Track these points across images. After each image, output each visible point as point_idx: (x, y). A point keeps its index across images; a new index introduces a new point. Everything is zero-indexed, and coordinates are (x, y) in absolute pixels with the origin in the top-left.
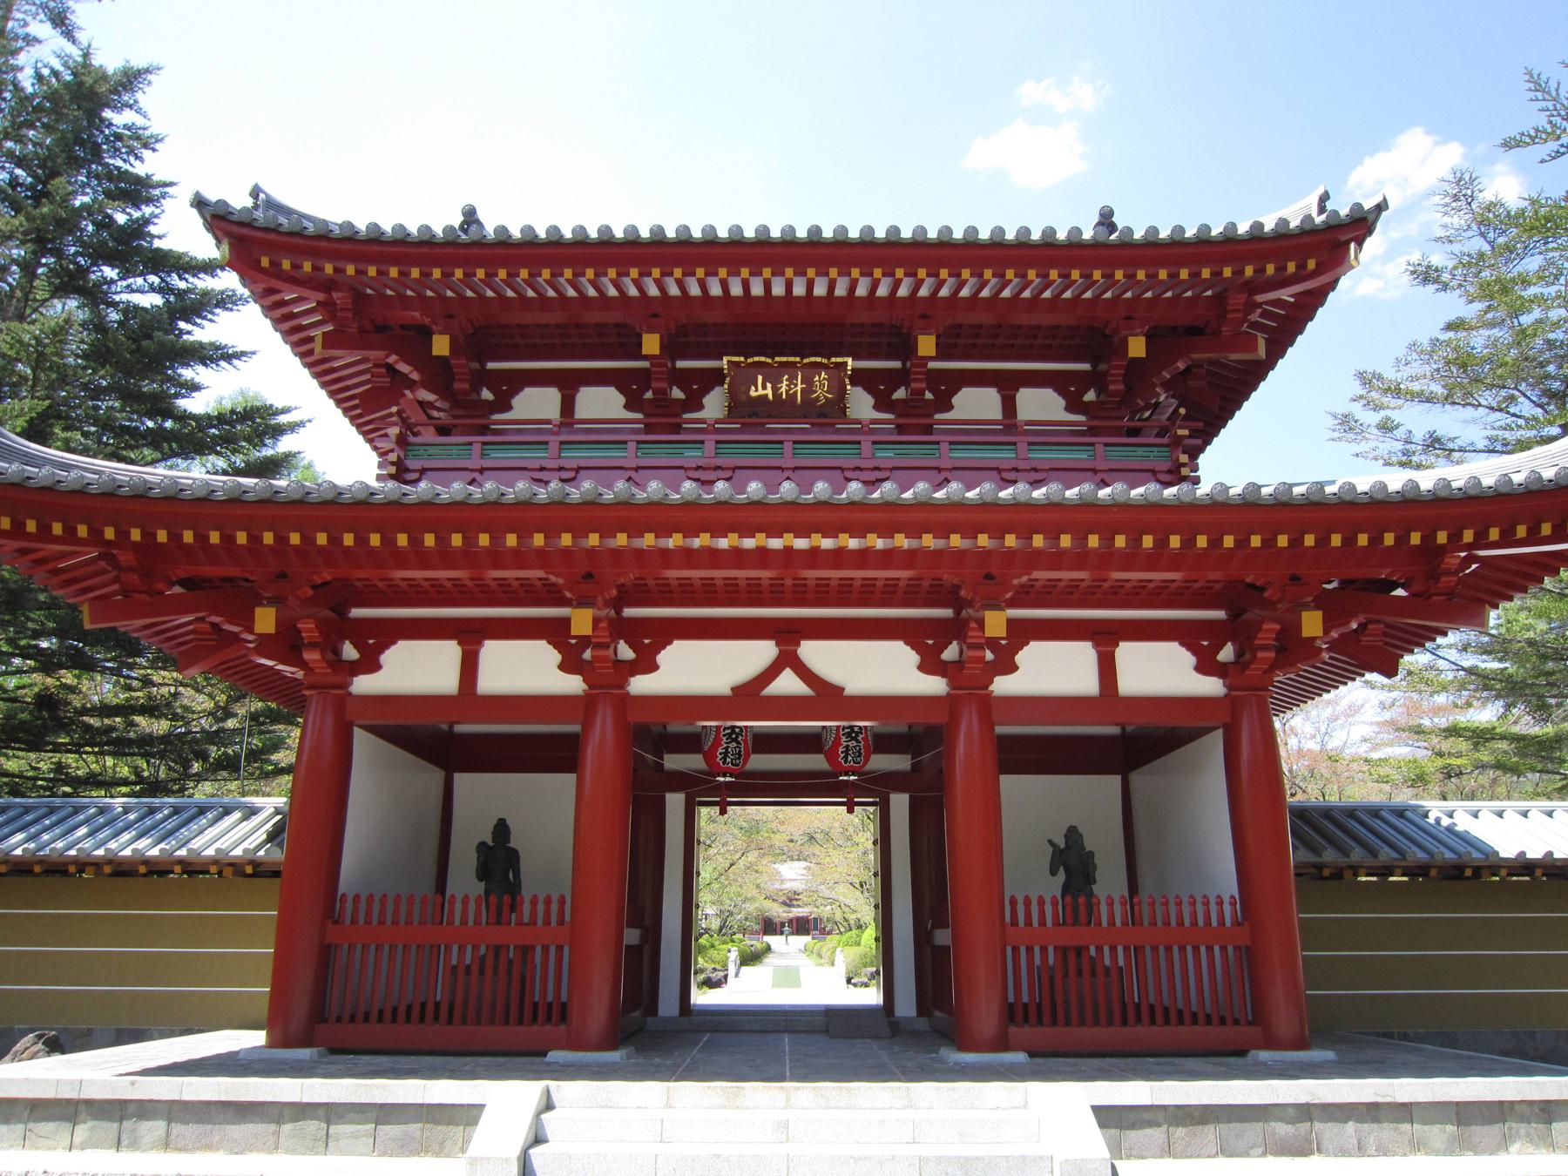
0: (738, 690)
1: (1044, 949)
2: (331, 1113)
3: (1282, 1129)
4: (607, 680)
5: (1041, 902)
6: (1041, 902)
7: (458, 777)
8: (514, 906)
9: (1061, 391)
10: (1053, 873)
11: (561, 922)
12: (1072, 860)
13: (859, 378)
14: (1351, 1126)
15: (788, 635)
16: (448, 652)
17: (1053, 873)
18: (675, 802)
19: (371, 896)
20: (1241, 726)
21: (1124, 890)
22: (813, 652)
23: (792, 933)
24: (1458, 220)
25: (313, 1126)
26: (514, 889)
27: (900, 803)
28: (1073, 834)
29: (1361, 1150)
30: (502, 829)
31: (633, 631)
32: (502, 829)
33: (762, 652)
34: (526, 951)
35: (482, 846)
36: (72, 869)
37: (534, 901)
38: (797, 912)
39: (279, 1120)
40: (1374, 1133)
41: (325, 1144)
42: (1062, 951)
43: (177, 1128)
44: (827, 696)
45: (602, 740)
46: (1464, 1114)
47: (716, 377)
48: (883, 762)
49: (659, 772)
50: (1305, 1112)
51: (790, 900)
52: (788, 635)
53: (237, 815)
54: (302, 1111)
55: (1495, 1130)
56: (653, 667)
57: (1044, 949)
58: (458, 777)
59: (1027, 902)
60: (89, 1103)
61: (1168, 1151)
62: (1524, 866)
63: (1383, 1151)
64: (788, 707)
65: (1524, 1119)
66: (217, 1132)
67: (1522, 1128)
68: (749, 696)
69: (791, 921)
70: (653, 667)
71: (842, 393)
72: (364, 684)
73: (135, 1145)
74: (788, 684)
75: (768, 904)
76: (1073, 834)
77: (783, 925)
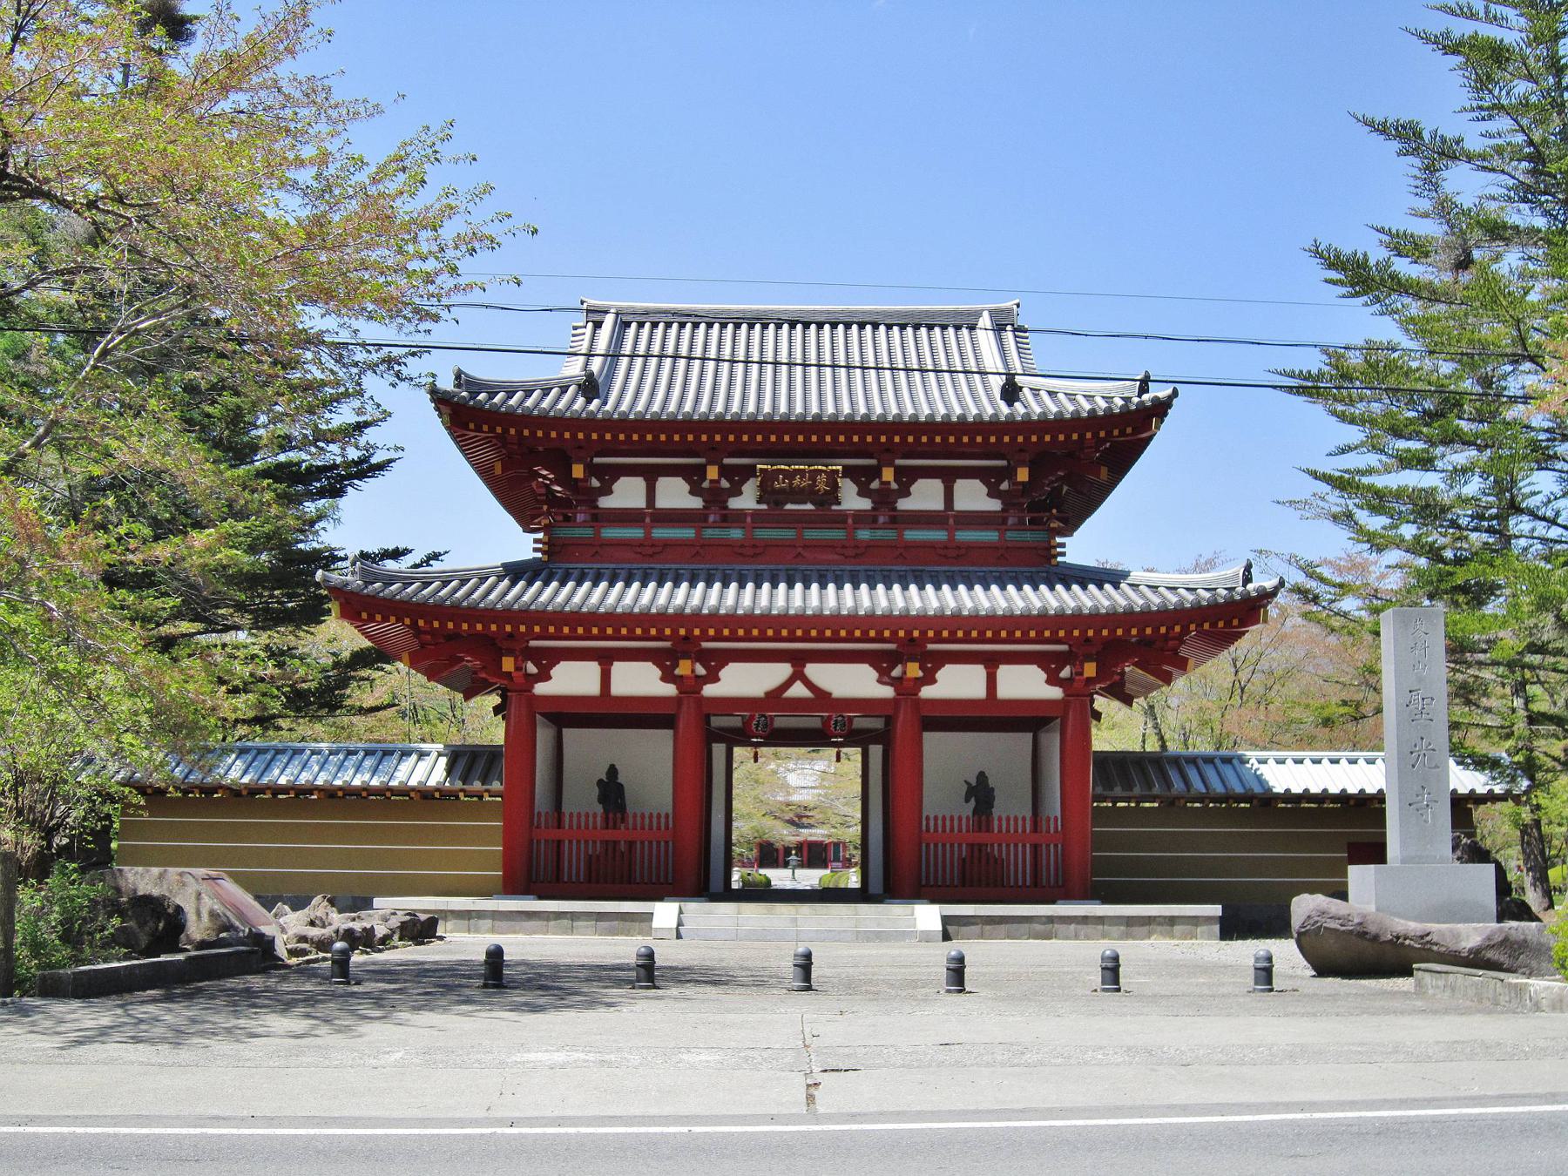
0: (768, 694)
1: (960, 846)
2: (574, 916)
3: (1038, 927)
4: (690, 687)
5: (960, 819)
6: (960, 819)
7: (565, 731)
8: (623, 820)
9: (985, 482)
10: (967, 801)
11: (667, 827)
12: (981, 793)
13: (849, 472)
14: (1073, 926)
15: (798, 660)
16: (592, 669)
17: (967, 801)
18: (719, 750)
19: (579, 815)
20: (1073, 715)
21: (1029, 815)
22: (813, 671)
23: (802, 865)
24: (1425, 204)
25: (566, 922)
26: (622, 808)
27: (876, 751)
28: (982, 776)
29: (1076, 937)
30: (613, 771)
31: (703, 657)
32: (613, 771)
33: (783, 670)
34: (631, 844)
35: (600, 782)
36: (340, 794)
37: (571, 815)
38: (817, 834)
39: (548, 920)
40: (1083, 929)
41: (572, 931)
42: (971, 846)
43: (497, 923)
44: (821, 697)
45: (686, 718)
46: (1130, 921)
47: (749, 472)
48: (861, 723)
49: (711, 735)
50: (1051, 920)
51: (798, 819)
52: (798, 660)
53: (414, 757)
54: (559, 915)
55: (1146, 928)
56: (717, 680)
57: (960, 846)
58: (565, 731)
59: (1008, 819)
60: (452, 912)
61: (982, 936)
62: (1288, 796)
63: (1087, 938)
64: (798, 703)
65: (1160, 924)
66: (517, 925)
67: (1159, 928)
68: (775, 697)
69: (800, 847)
70: (717, 680)
71: (835, 487)
72: (541, 689)
73: (477, 931)
74: (798, 690)
75: (769, 822)
76: (982, 776)
77: (787, 851)
